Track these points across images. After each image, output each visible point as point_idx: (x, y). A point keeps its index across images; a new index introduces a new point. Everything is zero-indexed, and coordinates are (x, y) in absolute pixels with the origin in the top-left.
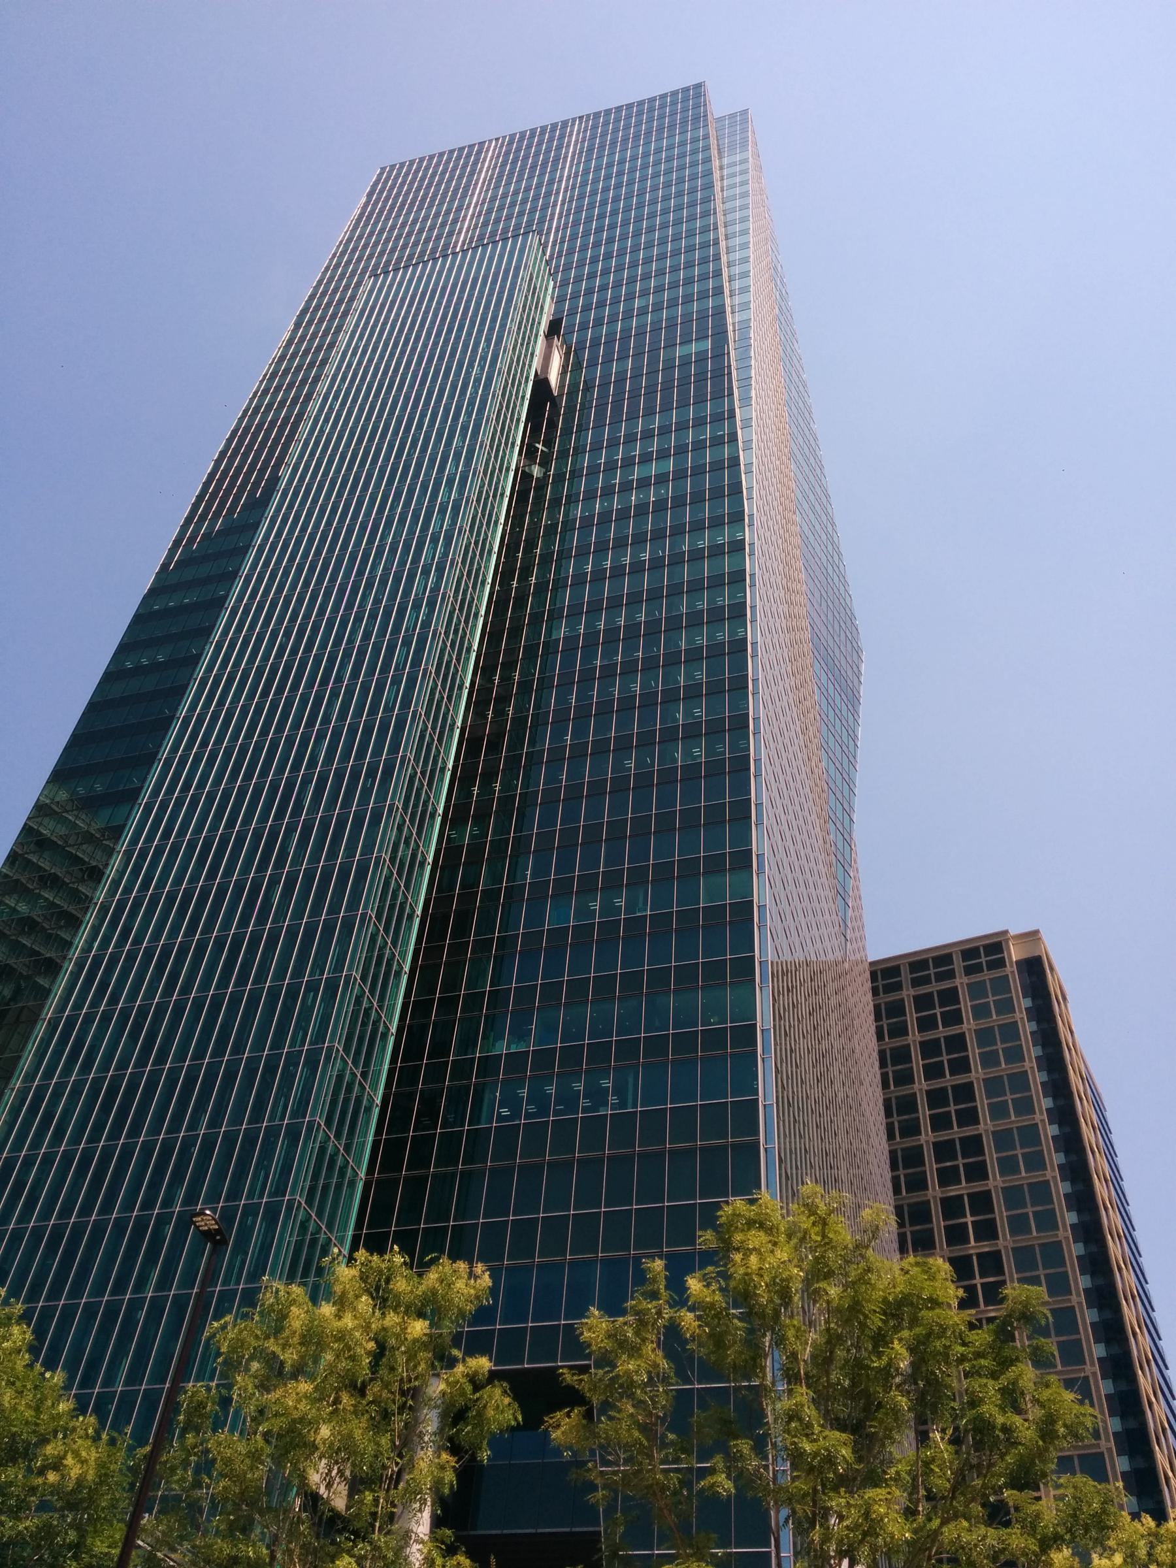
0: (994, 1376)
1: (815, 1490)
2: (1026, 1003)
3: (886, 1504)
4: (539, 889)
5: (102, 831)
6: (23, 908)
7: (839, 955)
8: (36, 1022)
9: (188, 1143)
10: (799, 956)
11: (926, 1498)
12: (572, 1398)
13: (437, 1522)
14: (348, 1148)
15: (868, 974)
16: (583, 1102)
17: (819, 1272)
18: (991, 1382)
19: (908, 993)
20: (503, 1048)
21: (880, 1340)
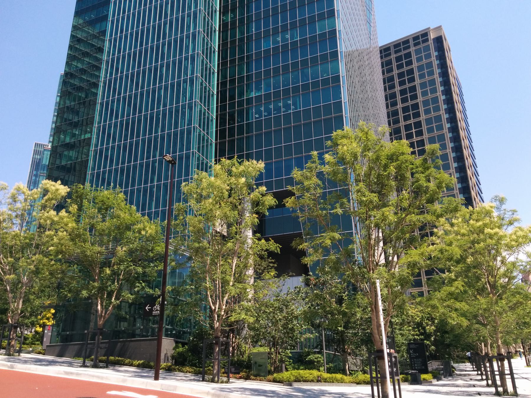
0: (423, 173)
1: (367, 211)
2: (436, 54)
3: (390, 213)
4: (258, 35)
5: (99, 33)
6: (80, 65)
7: (368, 46)
8: (96, 104)
9: (156, 138)
10: (354, 48)
11: (400, 209)
12: (290, 194)
13: (254, 233)
14: (207, 133)
15: (379, 52)
16: (283, 109)
17: (366, 149)
18: (422, 175)
19: (393, 56)
20: (253, 95)
21: (386, 167)
